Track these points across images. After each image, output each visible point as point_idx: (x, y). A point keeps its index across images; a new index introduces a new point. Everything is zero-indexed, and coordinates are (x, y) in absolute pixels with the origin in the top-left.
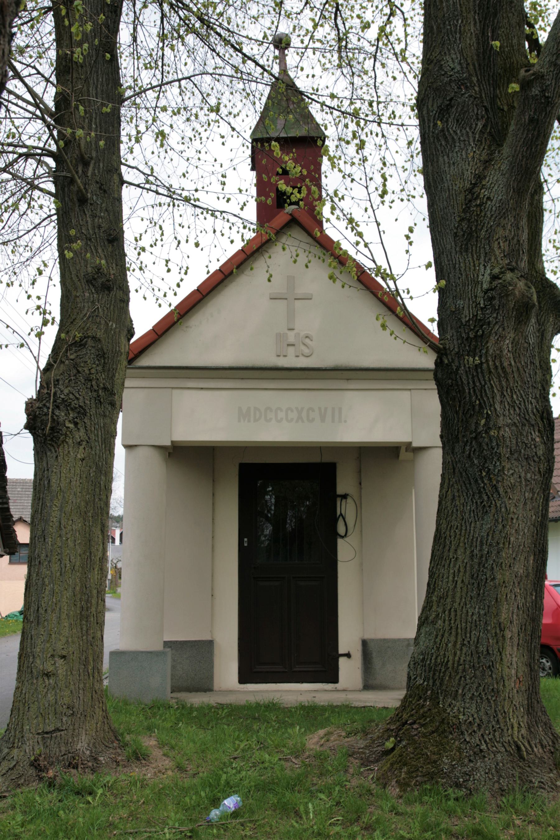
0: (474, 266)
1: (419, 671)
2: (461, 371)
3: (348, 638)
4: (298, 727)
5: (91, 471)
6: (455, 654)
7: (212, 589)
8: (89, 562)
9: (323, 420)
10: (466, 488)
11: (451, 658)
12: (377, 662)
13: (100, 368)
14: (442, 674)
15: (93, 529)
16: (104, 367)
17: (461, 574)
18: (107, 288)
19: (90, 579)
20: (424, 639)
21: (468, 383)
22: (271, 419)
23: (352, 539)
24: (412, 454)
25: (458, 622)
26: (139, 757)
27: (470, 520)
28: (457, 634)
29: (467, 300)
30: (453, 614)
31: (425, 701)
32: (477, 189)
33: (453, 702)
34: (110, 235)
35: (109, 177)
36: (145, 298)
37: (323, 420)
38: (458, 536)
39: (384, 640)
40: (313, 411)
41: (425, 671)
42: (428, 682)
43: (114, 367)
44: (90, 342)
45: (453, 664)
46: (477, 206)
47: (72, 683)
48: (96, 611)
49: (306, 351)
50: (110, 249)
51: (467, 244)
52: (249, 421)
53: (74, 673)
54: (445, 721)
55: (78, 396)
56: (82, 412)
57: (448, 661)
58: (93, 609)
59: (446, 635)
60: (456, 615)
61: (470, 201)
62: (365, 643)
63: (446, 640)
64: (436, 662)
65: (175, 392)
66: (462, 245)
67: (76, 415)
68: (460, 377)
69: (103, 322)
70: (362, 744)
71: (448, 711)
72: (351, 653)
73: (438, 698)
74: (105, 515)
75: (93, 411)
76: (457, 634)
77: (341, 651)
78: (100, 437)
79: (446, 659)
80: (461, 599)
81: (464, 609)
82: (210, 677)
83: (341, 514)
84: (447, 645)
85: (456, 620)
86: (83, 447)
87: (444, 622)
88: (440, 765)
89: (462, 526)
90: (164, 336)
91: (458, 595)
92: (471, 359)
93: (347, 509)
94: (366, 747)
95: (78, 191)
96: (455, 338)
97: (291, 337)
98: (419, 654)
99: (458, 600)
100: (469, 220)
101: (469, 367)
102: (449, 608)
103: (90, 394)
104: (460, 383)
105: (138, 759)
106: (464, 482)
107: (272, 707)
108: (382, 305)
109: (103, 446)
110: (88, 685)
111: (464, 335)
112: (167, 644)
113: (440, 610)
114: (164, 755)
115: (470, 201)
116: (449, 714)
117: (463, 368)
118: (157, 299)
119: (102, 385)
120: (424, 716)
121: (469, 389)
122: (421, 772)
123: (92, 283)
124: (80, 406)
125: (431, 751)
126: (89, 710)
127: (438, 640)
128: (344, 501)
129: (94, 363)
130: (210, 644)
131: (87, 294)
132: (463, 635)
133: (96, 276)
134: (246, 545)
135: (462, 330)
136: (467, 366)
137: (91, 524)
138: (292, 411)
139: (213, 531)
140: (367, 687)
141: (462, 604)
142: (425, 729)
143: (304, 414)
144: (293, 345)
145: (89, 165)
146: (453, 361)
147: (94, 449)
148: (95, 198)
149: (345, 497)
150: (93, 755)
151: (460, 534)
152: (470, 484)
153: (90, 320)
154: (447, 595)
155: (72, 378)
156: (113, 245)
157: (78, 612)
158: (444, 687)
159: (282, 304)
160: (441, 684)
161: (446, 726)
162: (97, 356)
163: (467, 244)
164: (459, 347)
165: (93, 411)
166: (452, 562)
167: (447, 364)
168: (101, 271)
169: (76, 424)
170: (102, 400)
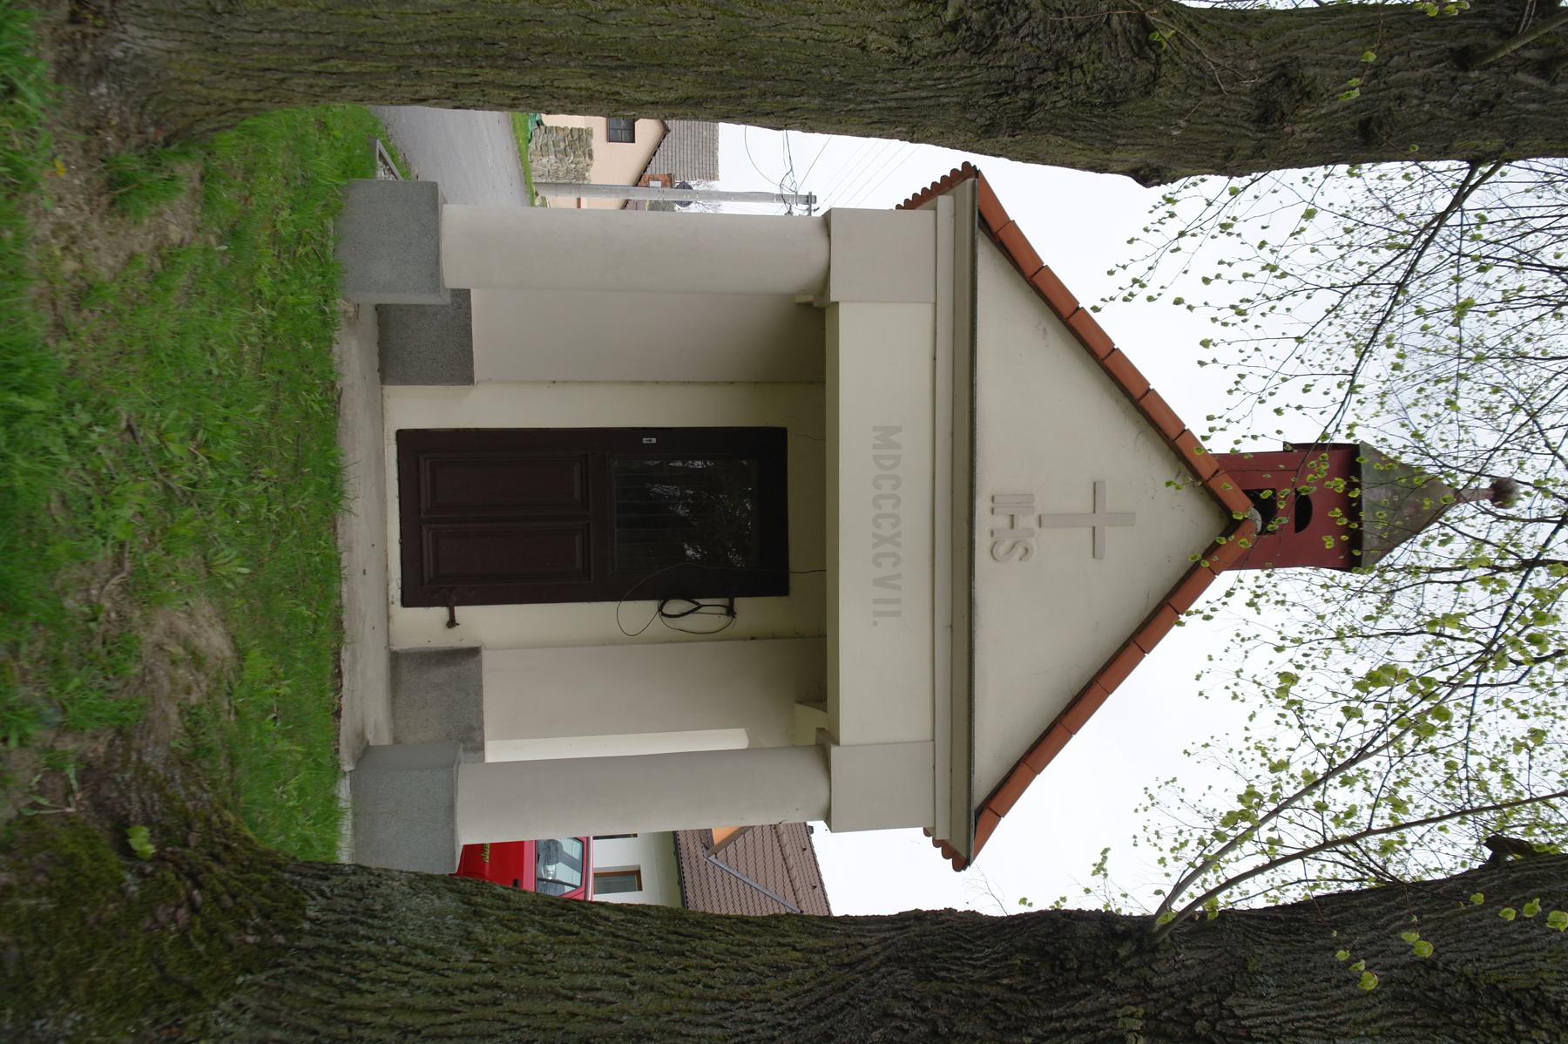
0: (1367, 1022)
1: (341, 903)
2: (1105, 998)
3: (484, 623)
4: (245, 571)
5: (835, 70)
6: (379, 1011)
7: (565, 382)
8: (608, 62)
9: (879, 582)
10: (808, 1007)
11: (369, 1000)
12: (440, 675)
13: (1081, 94)
14: (325, 975)
15: (690, 77)
16: (1083, 104)
17: (592, 1010)
18: (1267, 115)
19: (565, 65)
20: (425, 909)
21: (1075, 1016)
22: (878, 487)
23: (659, 626)
24: (813, 742)
25: (468, 1012)
26: (117, 193)
27: (728, 1024)
28: (433, 1011)
29: (1282, 1007)
30: (487, 995)
31: (258, 930)
32: (1547, 1021)
33: (249, 1016)
34: (1380, 127)
35: (1502, 127)
36: (1130, 242)
37: (879, 582)
38: (687, 991)
39: (481, 680)
40: (895, 565)
41: (339, 922)
42: (309, 933)
43: (1081, 133)
44: (1144, 68)
45: (352, 1008)
46: (1511, 1024)
47: (296, 11)
48: (486, 83)
49: (1002, 549)
50: (1347, 125)
51: (1413, 999)
52: (875, 447)
53: (324, 17)
54: (192, 1001)
55: (1022, 32)
56: (982, 44)
57: (360, 992)
58: (489, 74)
59: (432, 981)
60: (484, 1004)
61: (1519, 1004)
62: (474, 652)
63: (417, 982)
64: (361, 954)
65: (929, 308)
66: (1407, 984)
67: (975, 27)
68: (1088, 994)
69: (1188, 103)
70: (154, 756)
71: (222, 1004)
72: (456, 629)
73: (263, 969)
74: (724, 108)
75: (981, 75)
76: (433, 1011)
77: (458, 610)
78: (916, 94)
79: (365, 986)
80: (526, 1015)
81: (499, 1026)
82: (405, 380)
83: (700, 606)
84: (405, 984)
85: (472, 1005)
86: (896, 46)
87: (467, 971)
88: (55, 1007)
89: (714, 1000)
90: (1028, 287)
91: (538, 1006)
92: (1138, 1025)
93: (709, 616)
94: (142, 769)
95: (1485, 47)
96: (1184, 975)
97: (1027, 521)
98: (386, 897)
99: (524, 1006)
100: (1473, 1003)
101: (1115, 1018)
102: (504, 983)
103: (1024, 66)
104: (1073, 992)
105: (111, 184)
106: (822, 999)
107: (331, 493)
108: (1111, 654)
109: (892, 104)
110: (296, 57)
111: (1196, 1004)
112: (462, 296)
113: (498, 955)
114: (132, 257)
115: (1519, 1004)
116: (215, 1007)
117: (1113, 1000)
118: (1124, 267)
119: (1040, 98)
120: (212, 932)
121: (1060, 1019)
122: (35, 955)
123: (1278, 77)
124: (997, 38)
125: (100, 973)
126: (233, 61)
127: (422, 957)
128: (723, 610)
129: (1095, 79)
130: (467, 378)
131: (1252, 65)
132: (432, 1031)
133: (1294, 87)
134: (645, 440)
135: (1208, 998)
136: (1119, 1013)
137: (703, 69)
138: (894, 526)
139: (667, 383)
140: (397, 660)
141: (512, 1019)
142: (174, 944)
143: (887, 548)
144: (1012, 526)
145: (1538, 76)
146: (1128, 972)
147: (888, 77)
148: (1467, 88)
149: (731, 612)
150: (113, 67)
151: (692, 998)
152: (819, 1019)
153: (1195, 72)
154: (535, 974)
155: (1066, 18)
156: (1354, 133)
157: (481, 33)
158: (290, 984)
159: (1083, 503)
160: (301, 973)
161: (178, 1004)
162: (1111, 88)
163: (1413, 999)
164: (1163, 988)
165: (981, 75)
166: (621, 981)
167: (1116, 954)
168: (1306, 102)
169: (953, 27)
170: (1006, 99)
